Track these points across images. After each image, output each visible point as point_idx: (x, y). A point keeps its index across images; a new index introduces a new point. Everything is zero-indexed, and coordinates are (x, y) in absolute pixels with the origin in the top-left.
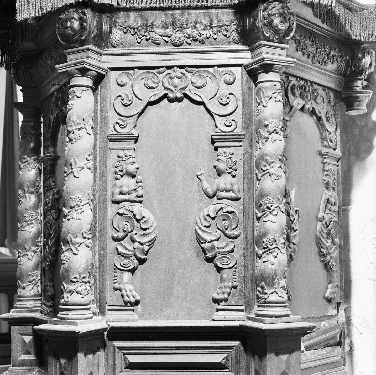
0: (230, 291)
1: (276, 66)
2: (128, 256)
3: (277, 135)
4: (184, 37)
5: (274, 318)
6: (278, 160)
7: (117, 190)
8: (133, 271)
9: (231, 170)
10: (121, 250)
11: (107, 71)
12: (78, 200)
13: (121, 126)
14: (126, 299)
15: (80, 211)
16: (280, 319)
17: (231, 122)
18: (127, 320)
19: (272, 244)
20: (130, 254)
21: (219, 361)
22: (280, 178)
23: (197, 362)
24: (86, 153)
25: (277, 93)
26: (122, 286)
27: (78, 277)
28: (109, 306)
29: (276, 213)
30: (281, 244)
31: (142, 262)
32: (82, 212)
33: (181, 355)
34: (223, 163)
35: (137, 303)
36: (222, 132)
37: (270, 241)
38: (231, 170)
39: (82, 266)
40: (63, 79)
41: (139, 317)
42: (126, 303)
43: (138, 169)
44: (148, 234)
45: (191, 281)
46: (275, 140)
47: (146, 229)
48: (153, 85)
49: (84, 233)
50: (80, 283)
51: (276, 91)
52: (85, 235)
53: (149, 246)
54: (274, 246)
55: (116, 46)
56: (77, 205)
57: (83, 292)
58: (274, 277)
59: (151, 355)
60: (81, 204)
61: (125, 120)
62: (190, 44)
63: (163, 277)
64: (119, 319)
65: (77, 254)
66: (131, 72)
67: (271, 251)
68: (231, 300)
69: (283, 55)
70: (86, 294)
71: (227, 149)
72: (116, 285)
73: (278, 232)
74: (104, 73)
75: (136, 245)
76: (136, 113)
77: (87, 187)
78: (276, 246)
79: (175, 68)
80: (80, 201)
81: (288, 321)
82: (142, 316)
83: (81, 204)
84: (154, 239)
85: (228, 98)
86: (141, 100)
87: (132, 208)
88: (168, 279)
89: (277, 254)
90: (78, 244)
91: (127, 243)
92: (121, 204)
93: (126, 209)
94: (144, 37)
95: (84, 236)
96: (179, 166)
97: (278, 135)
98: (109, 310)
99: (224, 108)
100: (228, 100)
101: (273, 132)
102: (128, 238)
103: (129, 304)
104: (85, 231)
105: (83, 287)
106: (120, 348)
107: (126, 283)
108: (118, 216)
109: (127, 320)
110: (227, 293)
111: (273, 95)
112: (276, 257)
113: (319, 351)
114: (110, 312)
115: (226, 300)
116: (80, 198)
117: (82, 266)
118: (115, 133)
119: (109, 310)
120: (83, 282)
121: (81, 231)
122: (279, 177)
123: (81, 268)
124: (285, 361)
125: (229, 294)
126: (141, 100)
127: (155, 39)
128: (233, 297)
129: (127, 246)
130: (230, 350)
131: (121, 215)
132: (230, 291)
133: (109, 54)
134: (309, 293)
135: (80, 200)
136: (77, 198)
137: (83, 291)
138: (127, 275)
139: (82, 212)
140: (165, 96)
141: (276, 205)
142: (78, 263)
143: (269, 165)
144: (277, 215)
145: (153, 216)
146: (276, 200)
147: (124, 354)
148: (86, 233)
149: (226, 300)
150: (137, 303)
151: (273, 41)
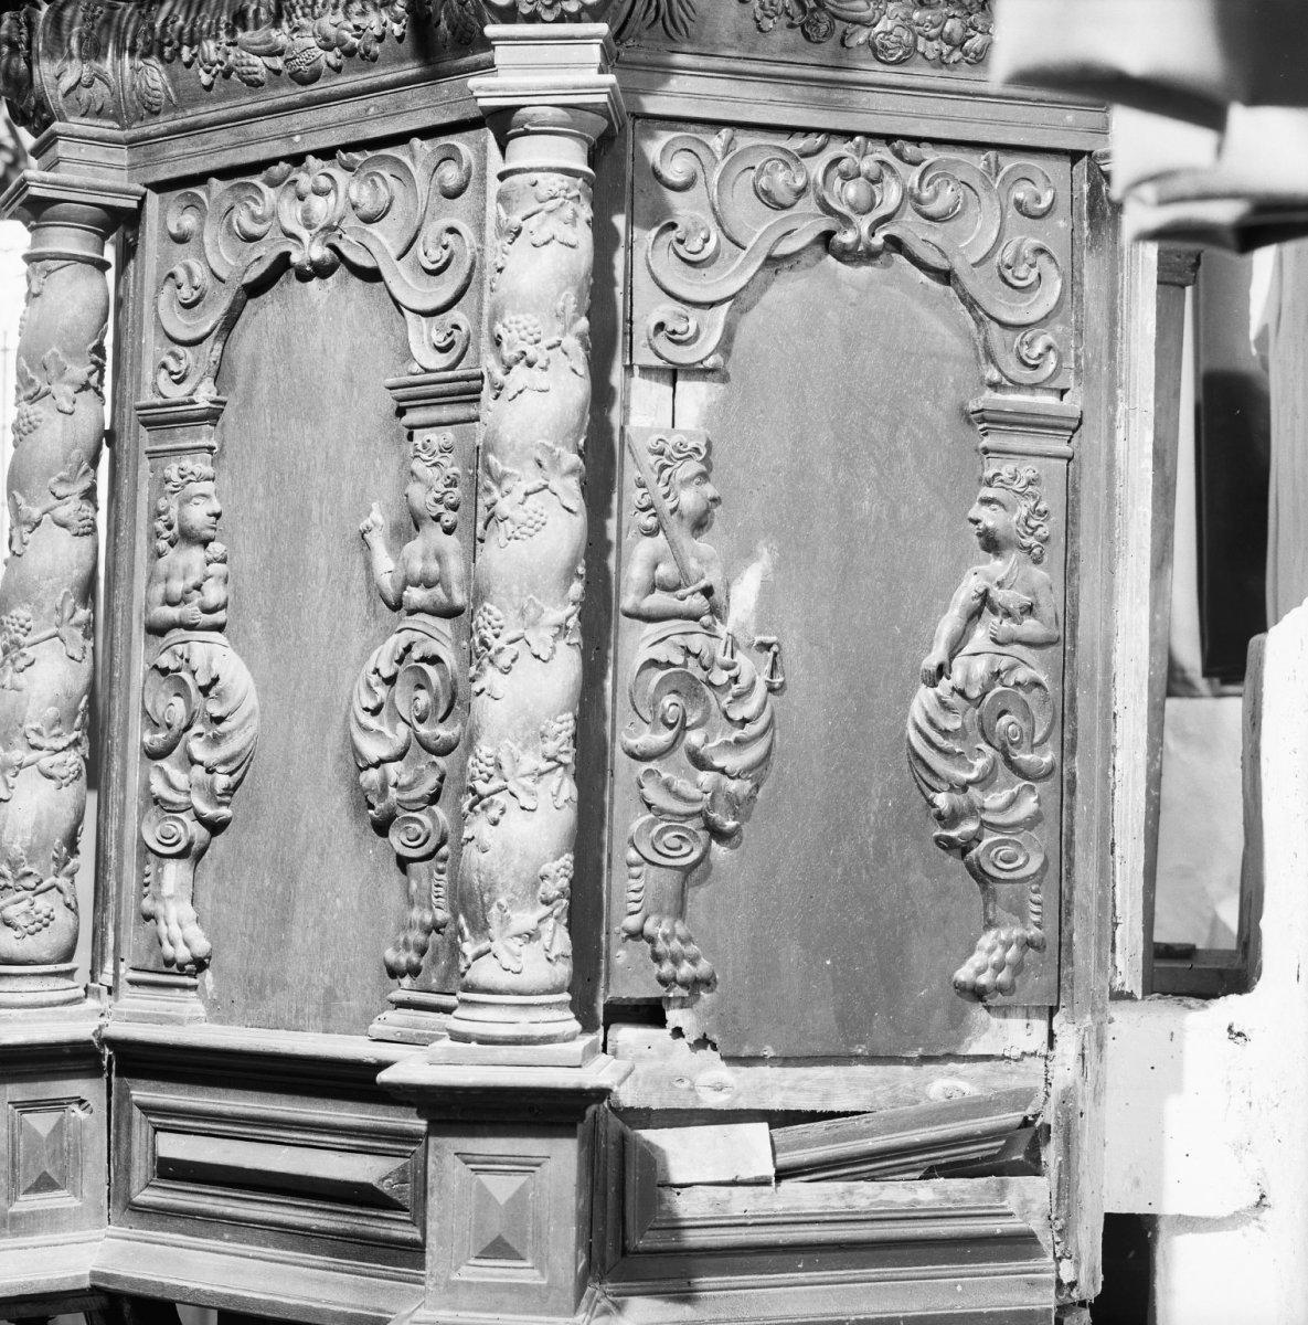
0: (1022, 959)
1: (522, 111)
2: (174, 808)
3: (532, 370)
4: (317, 49)
5: (474, 1045)
6: (532, 464)
7: (159, 591)
8: (191, 854)
9: (441, 508)
10: (158, 787)
11: (144, 196)
12: (17, 627)
13: (175, 377)
14: (168, 950)
15: (21, 663)
16: (491, 1050)
17: (449, 335)
18: (162, 1020)
19: (490, 776)
20: (180, 804)
21: (372, 1179)
22: (531, 531)
23: (317, 1179)
24: (51, 476)
25: (542, 214)
26: (159, 908)
27: (9, 874)
28: (135, 969)
29: (508, 663)
30: (524, 776)
31: (215, 827)
32: (513, 661)
33: (287, 1148)
34: (418, 485)
35: (200, 964)
36: (427, 371)
37: (482, 766)
38: (441, 508)
39: (19, 838)
40: (1081, 189)
41: (210, 1013)
42: (169, 962)
43: (218, 516)
44: (223, 735)
45: (338, 900)
46: (520, 392)
47: (219, 720)
48: (255, 229)
49: (32, 735)
50: (18, 891)
51: (539, 206)
52: (35, 739)
53: (231, 774)
54: (496, 783)
55: (156, 108)
56: (12, 642)
57: (21, 921)
58: (486, 899)
59: (261, 1145)
60: (28, 640)
61: (182, 354)
62: (338, 70)
63: (267, 882)
64: (143, 1015)
65: (7, 801)
66: (199, 191)
67: (486, 801)
68: (428, 972)
69: (582, 66)
70: (32, 928)
71: (437, 433)
72: (147, 904)
73: (511, 734)
74: (134, 205)
75: (198, 771)
76: (207, 329)
77: (46, 585)
78: (503, 783)
79: (310, 159)
80: (24, 630)
81: (523, 1061)
82: (219, 1011)
83: (28, 640)
84: (239, 754)
85: (445, 247)
86: (223, 282)
87: (189, 650)
88: (280, 889)
89: (503, 811)
90: (12, 767)
91: (678, 769)
92: (168, 636)
93: (675, 645)
94: (218, 66)
95: (33, 742)
96: (321, 501)
97: (535, 371)
98: (132, 983)
99: (438, 284)
100: (446, 254)
101: (517, 361)
102: (681, 755)
103: (174, 969)
104: (36, 725)
105: (24, 905)
106: (147, 1109)
107: (171, 897)
108: (156, 674)
109: (162, 1020)
110: (416, 945)
111: (524, 224)
112: (495, 823)
113: (883, 1188)
114: (135, 989)
115: (414, 971)
116: (22, 621)
117: (19, 838)
118: (159, 401)
119: (132, 983)
120: (26, 889)
121: (21, 726)
122: (524, 529)
123: (17, 846)
124: (502, 1203)
125: (422, 951)
126: (223, 282)
127: (250, 69)
128: (435, 961)
129: (172, 777)
130: (413, 1148)
131: (165, 672)
132: (1022, 959)
133: (938, 91)
134: (833, 963)
135: (22, 626)
136: (15, 620)
137: (23, 917)
138: (175, 874)
139: (513, 661)
140: (283, 262)
141: (513, 635)
142: (7, 828)
143: (499, 483)
144: (509, 668)
145: (247, 674)
146: (513, 615)
147: (156, 1130)
148: (38, 732)
149: (414, 971)
150: (200, 964)
151: (533, 18)
